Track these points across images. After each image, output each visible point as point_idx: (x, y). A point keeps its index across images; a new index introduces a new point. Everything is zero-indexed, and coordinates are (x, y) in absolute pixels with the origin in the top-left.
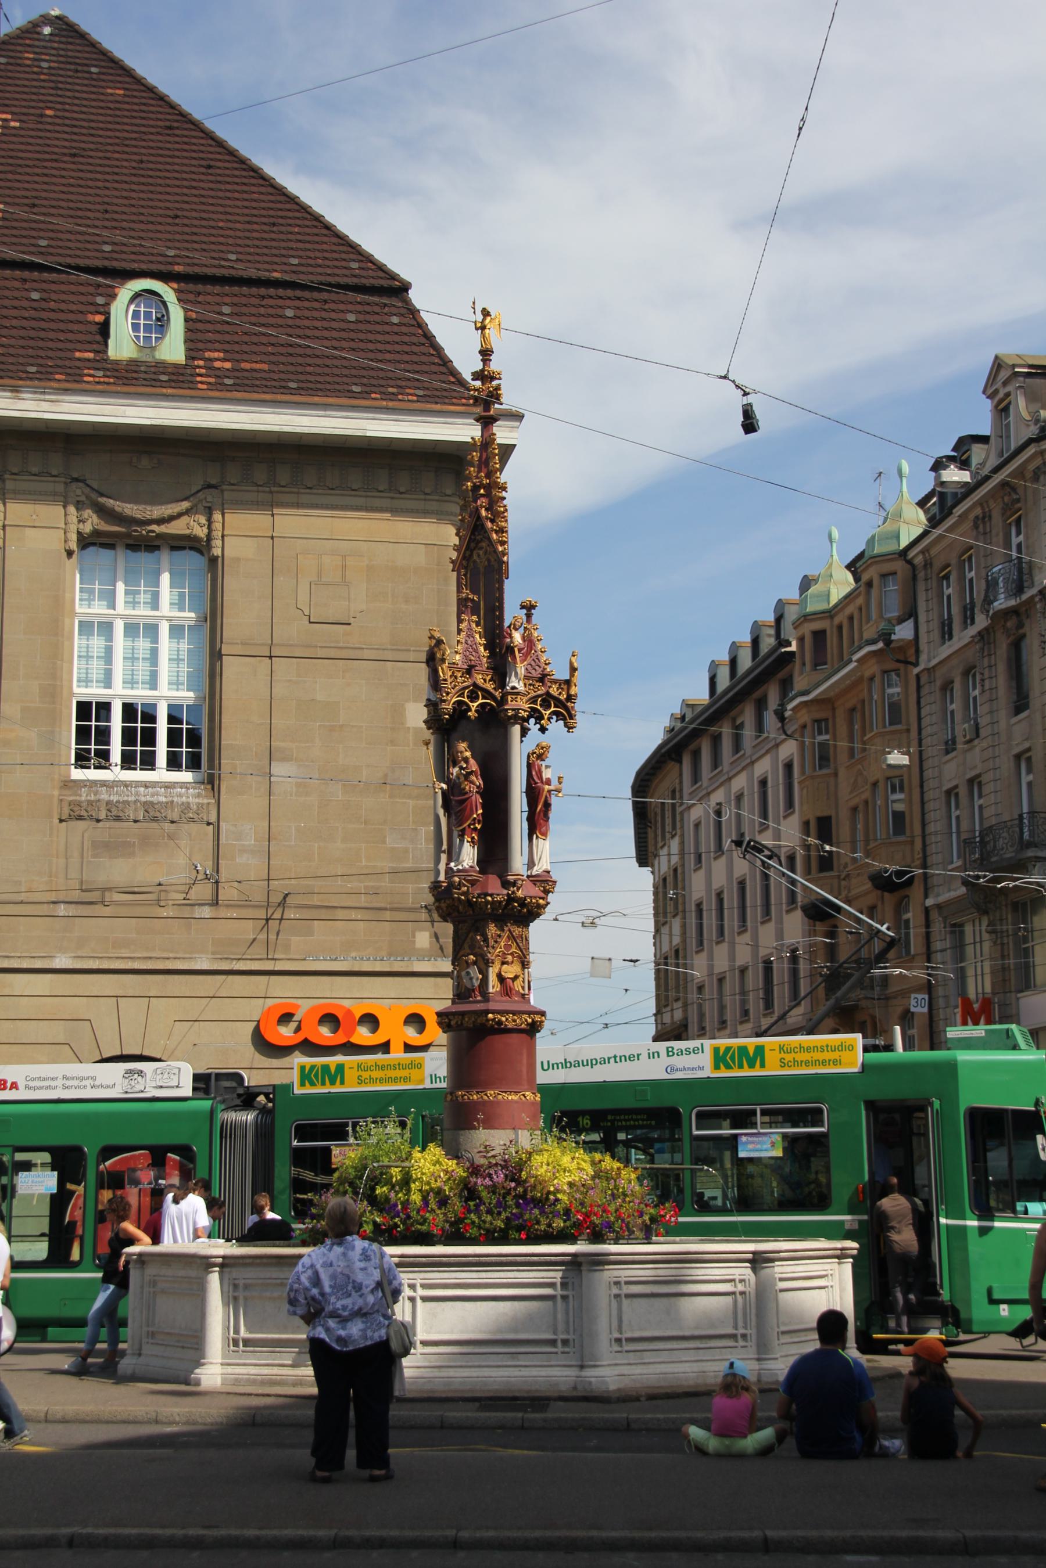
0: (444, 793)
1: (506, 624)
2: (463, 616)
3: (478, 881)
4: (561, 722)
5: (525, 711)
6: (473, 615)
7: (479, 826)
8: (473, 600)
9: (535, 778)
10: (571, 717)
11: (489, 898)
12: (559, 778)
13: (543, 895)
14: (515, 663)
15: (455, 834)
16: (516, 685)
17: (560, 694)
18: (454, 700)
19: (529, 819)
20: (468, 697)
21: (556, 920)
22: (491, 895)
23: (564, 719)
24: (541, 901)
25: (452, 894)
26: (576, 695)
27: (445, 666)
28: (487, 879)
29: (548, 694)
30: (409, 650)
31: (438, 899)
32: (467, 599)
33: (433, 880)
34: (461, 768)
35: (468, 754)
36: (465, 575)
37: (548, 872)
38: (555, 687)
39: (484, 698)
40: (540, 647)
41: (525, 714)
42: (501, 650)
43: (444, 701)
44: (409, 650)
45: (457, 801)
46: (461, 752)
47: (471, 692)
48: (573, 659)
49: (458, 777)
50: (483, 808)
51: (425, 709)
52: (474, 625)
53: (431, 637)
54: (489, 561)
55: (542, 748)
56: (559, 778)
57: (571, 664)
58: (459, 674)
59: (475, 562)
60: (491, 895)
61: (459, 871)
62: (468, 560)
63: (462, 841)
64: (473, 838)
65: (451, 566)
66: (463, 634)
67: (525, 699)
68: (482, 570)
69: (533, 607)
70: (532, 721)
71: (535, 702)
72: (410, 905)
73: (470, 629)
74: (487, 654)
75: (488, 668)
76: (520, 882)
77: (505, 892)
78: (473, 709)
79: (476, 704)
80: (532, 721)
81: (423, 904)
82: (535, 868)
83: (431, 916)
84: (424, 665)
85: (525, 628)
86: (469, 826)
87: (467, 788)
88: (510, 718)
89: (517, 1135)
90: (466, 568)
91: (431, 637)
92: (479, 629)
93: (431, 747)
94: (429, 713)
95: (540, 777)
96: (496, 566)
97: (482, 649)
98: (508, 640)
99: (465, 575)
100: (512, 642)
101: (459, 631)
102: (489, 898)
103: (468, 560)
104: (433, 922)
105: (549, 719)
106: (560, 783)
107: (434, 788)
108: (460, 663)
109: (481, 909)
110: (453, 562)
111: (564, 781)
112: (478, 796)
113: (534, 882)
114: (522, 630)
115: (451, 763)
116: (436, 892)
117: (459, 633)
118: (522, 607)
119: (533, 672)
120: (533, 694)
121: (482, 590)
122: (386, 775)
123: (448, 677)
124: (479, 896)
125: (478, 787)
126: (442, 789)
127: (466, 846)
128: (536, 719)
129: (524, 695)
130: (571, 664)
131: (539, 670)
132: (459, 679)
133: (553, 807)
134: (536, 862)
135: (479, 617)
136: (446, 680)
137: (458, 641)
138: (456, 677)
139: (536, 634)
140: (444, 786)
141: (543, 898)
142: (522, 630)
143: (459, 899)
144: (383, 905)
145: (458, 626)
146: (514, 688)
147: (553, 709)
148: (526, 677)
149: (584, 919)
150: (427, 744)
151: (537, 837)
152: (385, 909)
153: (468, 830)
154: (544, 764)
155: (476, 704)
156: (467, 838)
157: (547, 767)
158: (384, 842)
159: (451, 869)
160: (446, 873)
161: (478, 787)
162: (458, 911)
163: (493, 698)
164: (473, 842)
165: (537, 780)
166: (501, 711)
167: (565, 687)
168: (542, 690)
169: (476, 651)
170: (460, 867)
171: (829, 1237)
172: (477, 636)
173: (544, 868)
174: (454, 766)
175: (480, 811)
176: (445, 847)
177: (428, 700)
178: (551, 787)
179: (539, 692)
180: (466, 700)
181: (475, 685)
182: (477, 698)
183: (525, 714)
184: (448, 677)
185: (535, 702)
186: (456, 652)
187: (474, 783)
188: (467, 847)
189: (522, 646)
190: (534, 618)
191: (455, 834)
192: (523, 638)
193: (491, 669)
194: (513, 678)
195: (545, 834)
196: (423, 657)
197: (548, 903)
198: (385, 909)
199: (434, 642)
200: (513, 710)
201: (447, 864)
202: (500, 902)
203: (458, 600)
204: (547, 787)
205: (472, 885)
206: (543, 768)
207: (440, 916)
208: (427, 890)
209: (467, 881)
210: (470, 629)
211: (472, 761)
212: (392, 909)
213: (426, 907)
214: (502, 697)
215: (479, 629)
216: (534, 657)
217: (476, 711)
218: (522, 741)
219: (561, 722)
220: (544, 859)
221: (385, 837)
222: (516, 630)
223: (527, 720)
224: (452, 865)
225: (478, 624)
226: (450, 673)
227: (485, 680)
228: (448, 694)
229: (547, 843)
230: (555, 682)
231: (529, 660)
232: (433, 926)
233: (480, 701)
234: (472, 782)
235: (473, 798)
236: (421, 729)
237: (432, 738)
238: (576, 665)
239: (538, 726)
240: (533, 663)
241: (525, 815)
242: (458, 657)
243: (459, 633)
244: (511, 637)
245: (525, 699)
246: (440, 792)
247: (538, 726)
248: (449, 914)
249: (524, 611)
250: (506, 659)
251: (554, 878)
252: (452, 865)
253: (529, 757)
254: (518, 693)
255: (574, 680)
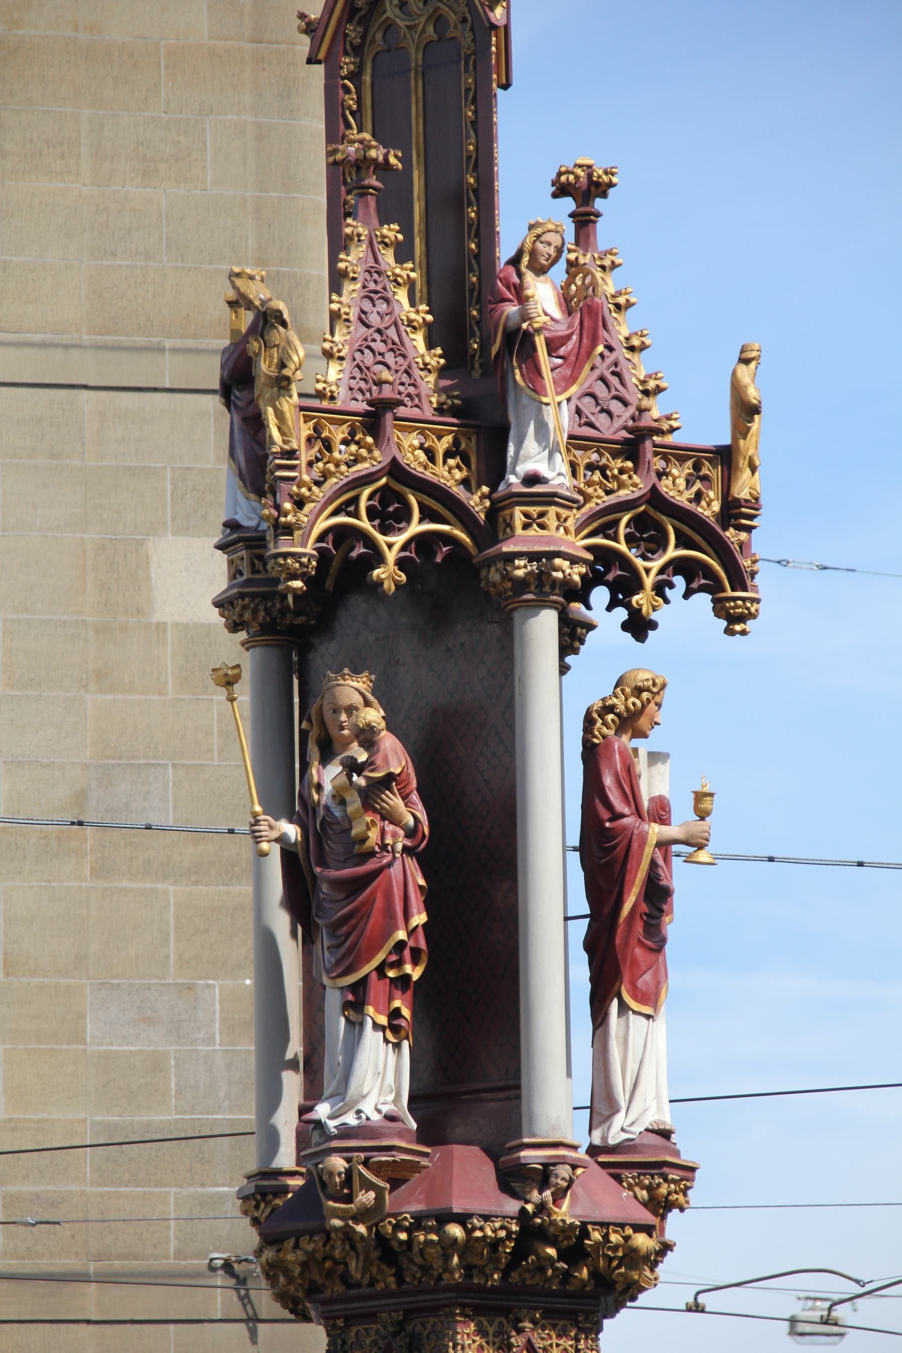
0: (289, 857)
1: (505, 251)
2: (352, 226)
3: (415, 1167)
4: (703, 600)
5: (574, 560)
6: (384, 220)
7: (415, 973)
8: (383, 167)
9: (615, 798)
10: (739, 579)
11: (456, 1231)
12: (700, 797)
13: (647, 1217)
14: (537, 389)
15: (333, 999)
16: (543, 469)
17: (698, 497)
18: (322, 525)
19: (590, 945)
20: (372, 514)
21: (696, 1308)
22: (462, 1219)
23: (714, 588)
24: (641, 1241)
25: (320, 1215)
26: (754, 503)
27: (289, 404)
28: (447, 1163)
29: (655, 497)
30: (161, 350)
31: (270, 1239)
32: (362, 164)
33: (253, 1166)
34: (353, 767)
35: (374, 715)
36: (355, 76)
37: (666, 1134)
38: (680, 472)
39: (428, 515)
40: (624, 331)
41: (576, 573)
42: (485, 345)
43: (289, 530)
44: (161, 350)
45: (338, 884)
46: (351, 710)
47: (385, 495)
48: (745, 374)
49: (340, 798)
50: (429, 906)
51: (221, 560)
52: (388, 257)
53: (238, 302)
54: (438, 21)
55: (638, 691)
56: (700, 797)
57: (737, 389)
58: (339, 434)
59: (389, 27)
60: (462, 1219)
61: (346, 1132)
62: (365, 22)
63: (356, 1026)
64: (395, 1014)
65: (304, 44)
66: (351, 290)
67: (574, 518)
68: (416, 57)
69: (600, 189)
70: (600, 595)
71: (608, 529)
72: (170, 1263)
73: (375, 271)
74: (435, 359)
75: (440, 410)
76: (564, 1171)
77: (512, 1206)
78: (391, 556)
79: (399, 539)
80: (600, 595)
81: (219, 1256)
82: (619, 1120)
83: (245, 1300)
84: (214, 403)
85: (572, 265)
86: (381, 970)
87: (374, 835)
88: (522, 585)
89: (279, 372)
90: (358, 50)
91: (238, 302)
92: (408, 271)
93: (244, 692)
94: (235, 573)
95: (632, 796)
96: (466, 41)
97: (419, 340)
98: (511, 309)
99: (355, 76)
100: (525, 316)
101: (337, 279)
102: (456, 1231)
103: (365, 22)
104: (253, 1320)
105: (660, 589)
106: (702, 815)
107: (257, 838)
108: (342, 393)
109: (426, 1269)
110: (309, 28)
111: (717, 806)
112: (412, 865)
113: (615, 1171)
114: (559, 272)
115: (313, 751)
116: (264, 1212)
117: (335, 286)
118: (561, 190)
119: (602, 420)
120: (600, 500)
121: (417, 127)
122: (81, 796)
123: (298, 443)
124: (419, 1222)
125: (411, 833)
126: (282, 840)
127: (372, 1040)
128: (614, 588)
129: (570, 503)
130: (737, 389)
131: (624, 415)
132: (341, 452)
133: (678, 900)
134: (622, 1099)
135: (407, 229)
136: (291, 454)
137: (335, 316)
138: (328, 445)
139: (609, 285)
140: (292, 831)
141: (648, 1230)
142: (559, 272)
143: (348, 1235)
144: (73, 1264)
145: (333, 260)
146: (533, 479)
147: (672, 552)
148: (576, 441)
149: (796, 1309)
150: (229, 682)
151: (623, 1008)
152: (83, 1278)
153: (377, 988)
154: (643, 746)
155: (399, 539)
156: (374, 1015)
157: (655, 758)
158: (78, 1037)
159: (319, 1125)
160: (302, 1141)
161: (411, 833)
162: (345, 1278)
163: (462, 514)
164: (395, 1029)
165: (620, 806)
166: (489, 562)
167: (715, 473)
168: (377, 460)
169: (399, 349)
170: (350, 1119)
171: (331, 504)
172: (402, 296)
173: (648, 1120)
174: (325, 760)
175: (419, 918)
176: (295, 1048)
177: (232, 525)
178: (671, 831)
179: (624, 494)
180: (365, 524)
181: (395, 469)
182: (404, 516)
183: (576, 573)
184: (298, 443)
185: (608, 529)
186: (328, 355)
187: (396, 822)
188: (372, 1040)
189: (561, 330)
190: (602, 227)
191: (333, 999)
192: (566, 302)
193: (454, 411)
194: (531, 445)
195: (651, 998)
196: (213, 377)
197: (666, 1248)
198: (83, 1278)
199: (247, 318)
200: (532, 557)
201: (304, 1110)
202: (495, 1244)
203: (333, 165)
204: (655, 831)
205: (396, 1184)
206: (641, 764)
207: (282, 1298)
208: (234, 1207)
209: (378, 1169)
210: (375, 271)
211: (389, 742)
212: (105, 1279)
213: (227, 1266)
214: (492, 514)
215: (408, 271)
216: (604, 368)
217: (401, 563)
218: (564, 669)
219: (703, 600)
220: (647, 1087)
221: (82, 1016)
222: (540, 271)
223: (581, 594)
224: (322, 1111)
225: (403, 253)
226: (306, 430)
227: (431, 454)
228: (300, 503)
229: (660, 1027)
230: (681, 454)
231: (586, 379)
232: (253, 1336)
233: (416, 527)
234: (389, 816)
235: (396, 871)
236: (207, 628)
237: (247, 661)
238: (753, 394)
239: (621, 614)
240: (600, 390)
241: (580, 929)
242: (334, 371)
243: (335, 286)
244: (522, 298)
245: (574, 518)
246: (275, 851)
247: (621, 614)
248: (313, 1290)
249: (568, 204)
250: (505, 377)
251: (686, 1158)
252: (322, 1111)
253: (589, 722)
254: (550, 499)
255: (747, 446)
